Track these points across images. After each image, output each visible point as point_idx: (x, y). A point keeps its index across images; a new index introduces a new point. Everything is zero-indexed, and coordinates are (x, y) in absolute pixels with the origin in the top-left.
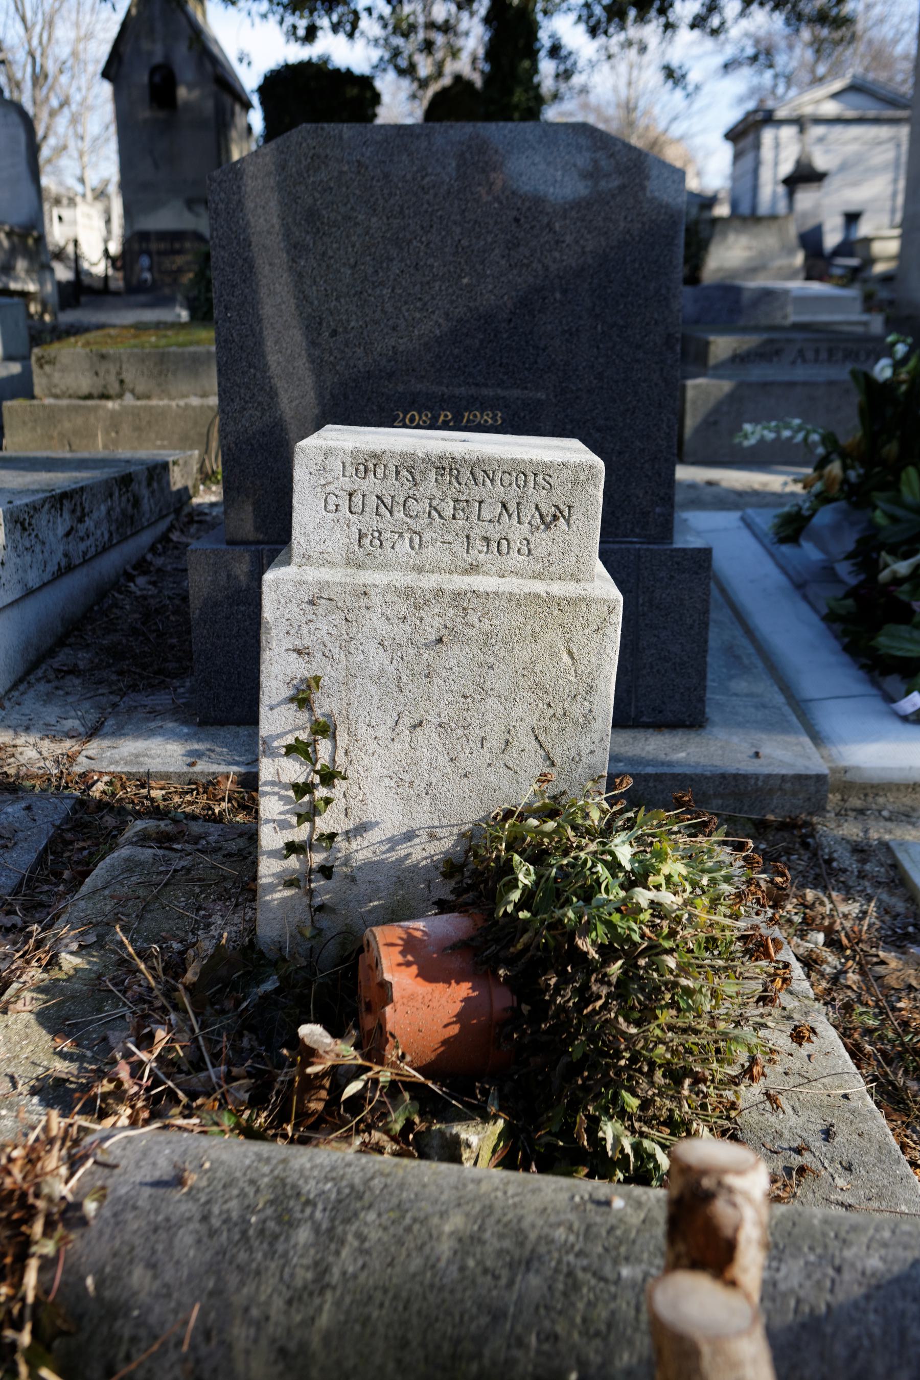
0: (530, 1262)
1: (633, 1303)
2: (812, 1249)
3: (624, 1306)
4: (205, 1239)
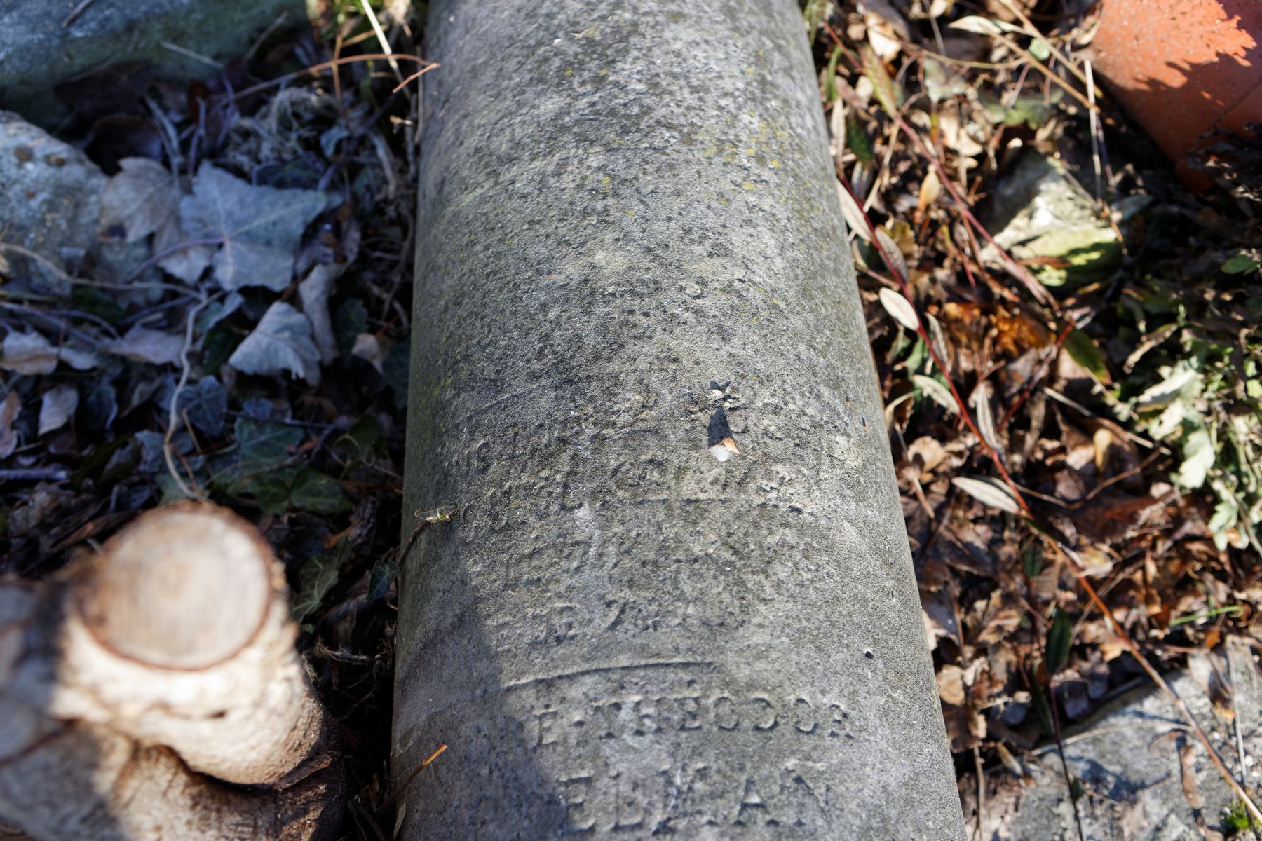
0: (569, 380)
1: (540, 544)
2: (702, 774)
3: (537, 533)
4: (523, 14)
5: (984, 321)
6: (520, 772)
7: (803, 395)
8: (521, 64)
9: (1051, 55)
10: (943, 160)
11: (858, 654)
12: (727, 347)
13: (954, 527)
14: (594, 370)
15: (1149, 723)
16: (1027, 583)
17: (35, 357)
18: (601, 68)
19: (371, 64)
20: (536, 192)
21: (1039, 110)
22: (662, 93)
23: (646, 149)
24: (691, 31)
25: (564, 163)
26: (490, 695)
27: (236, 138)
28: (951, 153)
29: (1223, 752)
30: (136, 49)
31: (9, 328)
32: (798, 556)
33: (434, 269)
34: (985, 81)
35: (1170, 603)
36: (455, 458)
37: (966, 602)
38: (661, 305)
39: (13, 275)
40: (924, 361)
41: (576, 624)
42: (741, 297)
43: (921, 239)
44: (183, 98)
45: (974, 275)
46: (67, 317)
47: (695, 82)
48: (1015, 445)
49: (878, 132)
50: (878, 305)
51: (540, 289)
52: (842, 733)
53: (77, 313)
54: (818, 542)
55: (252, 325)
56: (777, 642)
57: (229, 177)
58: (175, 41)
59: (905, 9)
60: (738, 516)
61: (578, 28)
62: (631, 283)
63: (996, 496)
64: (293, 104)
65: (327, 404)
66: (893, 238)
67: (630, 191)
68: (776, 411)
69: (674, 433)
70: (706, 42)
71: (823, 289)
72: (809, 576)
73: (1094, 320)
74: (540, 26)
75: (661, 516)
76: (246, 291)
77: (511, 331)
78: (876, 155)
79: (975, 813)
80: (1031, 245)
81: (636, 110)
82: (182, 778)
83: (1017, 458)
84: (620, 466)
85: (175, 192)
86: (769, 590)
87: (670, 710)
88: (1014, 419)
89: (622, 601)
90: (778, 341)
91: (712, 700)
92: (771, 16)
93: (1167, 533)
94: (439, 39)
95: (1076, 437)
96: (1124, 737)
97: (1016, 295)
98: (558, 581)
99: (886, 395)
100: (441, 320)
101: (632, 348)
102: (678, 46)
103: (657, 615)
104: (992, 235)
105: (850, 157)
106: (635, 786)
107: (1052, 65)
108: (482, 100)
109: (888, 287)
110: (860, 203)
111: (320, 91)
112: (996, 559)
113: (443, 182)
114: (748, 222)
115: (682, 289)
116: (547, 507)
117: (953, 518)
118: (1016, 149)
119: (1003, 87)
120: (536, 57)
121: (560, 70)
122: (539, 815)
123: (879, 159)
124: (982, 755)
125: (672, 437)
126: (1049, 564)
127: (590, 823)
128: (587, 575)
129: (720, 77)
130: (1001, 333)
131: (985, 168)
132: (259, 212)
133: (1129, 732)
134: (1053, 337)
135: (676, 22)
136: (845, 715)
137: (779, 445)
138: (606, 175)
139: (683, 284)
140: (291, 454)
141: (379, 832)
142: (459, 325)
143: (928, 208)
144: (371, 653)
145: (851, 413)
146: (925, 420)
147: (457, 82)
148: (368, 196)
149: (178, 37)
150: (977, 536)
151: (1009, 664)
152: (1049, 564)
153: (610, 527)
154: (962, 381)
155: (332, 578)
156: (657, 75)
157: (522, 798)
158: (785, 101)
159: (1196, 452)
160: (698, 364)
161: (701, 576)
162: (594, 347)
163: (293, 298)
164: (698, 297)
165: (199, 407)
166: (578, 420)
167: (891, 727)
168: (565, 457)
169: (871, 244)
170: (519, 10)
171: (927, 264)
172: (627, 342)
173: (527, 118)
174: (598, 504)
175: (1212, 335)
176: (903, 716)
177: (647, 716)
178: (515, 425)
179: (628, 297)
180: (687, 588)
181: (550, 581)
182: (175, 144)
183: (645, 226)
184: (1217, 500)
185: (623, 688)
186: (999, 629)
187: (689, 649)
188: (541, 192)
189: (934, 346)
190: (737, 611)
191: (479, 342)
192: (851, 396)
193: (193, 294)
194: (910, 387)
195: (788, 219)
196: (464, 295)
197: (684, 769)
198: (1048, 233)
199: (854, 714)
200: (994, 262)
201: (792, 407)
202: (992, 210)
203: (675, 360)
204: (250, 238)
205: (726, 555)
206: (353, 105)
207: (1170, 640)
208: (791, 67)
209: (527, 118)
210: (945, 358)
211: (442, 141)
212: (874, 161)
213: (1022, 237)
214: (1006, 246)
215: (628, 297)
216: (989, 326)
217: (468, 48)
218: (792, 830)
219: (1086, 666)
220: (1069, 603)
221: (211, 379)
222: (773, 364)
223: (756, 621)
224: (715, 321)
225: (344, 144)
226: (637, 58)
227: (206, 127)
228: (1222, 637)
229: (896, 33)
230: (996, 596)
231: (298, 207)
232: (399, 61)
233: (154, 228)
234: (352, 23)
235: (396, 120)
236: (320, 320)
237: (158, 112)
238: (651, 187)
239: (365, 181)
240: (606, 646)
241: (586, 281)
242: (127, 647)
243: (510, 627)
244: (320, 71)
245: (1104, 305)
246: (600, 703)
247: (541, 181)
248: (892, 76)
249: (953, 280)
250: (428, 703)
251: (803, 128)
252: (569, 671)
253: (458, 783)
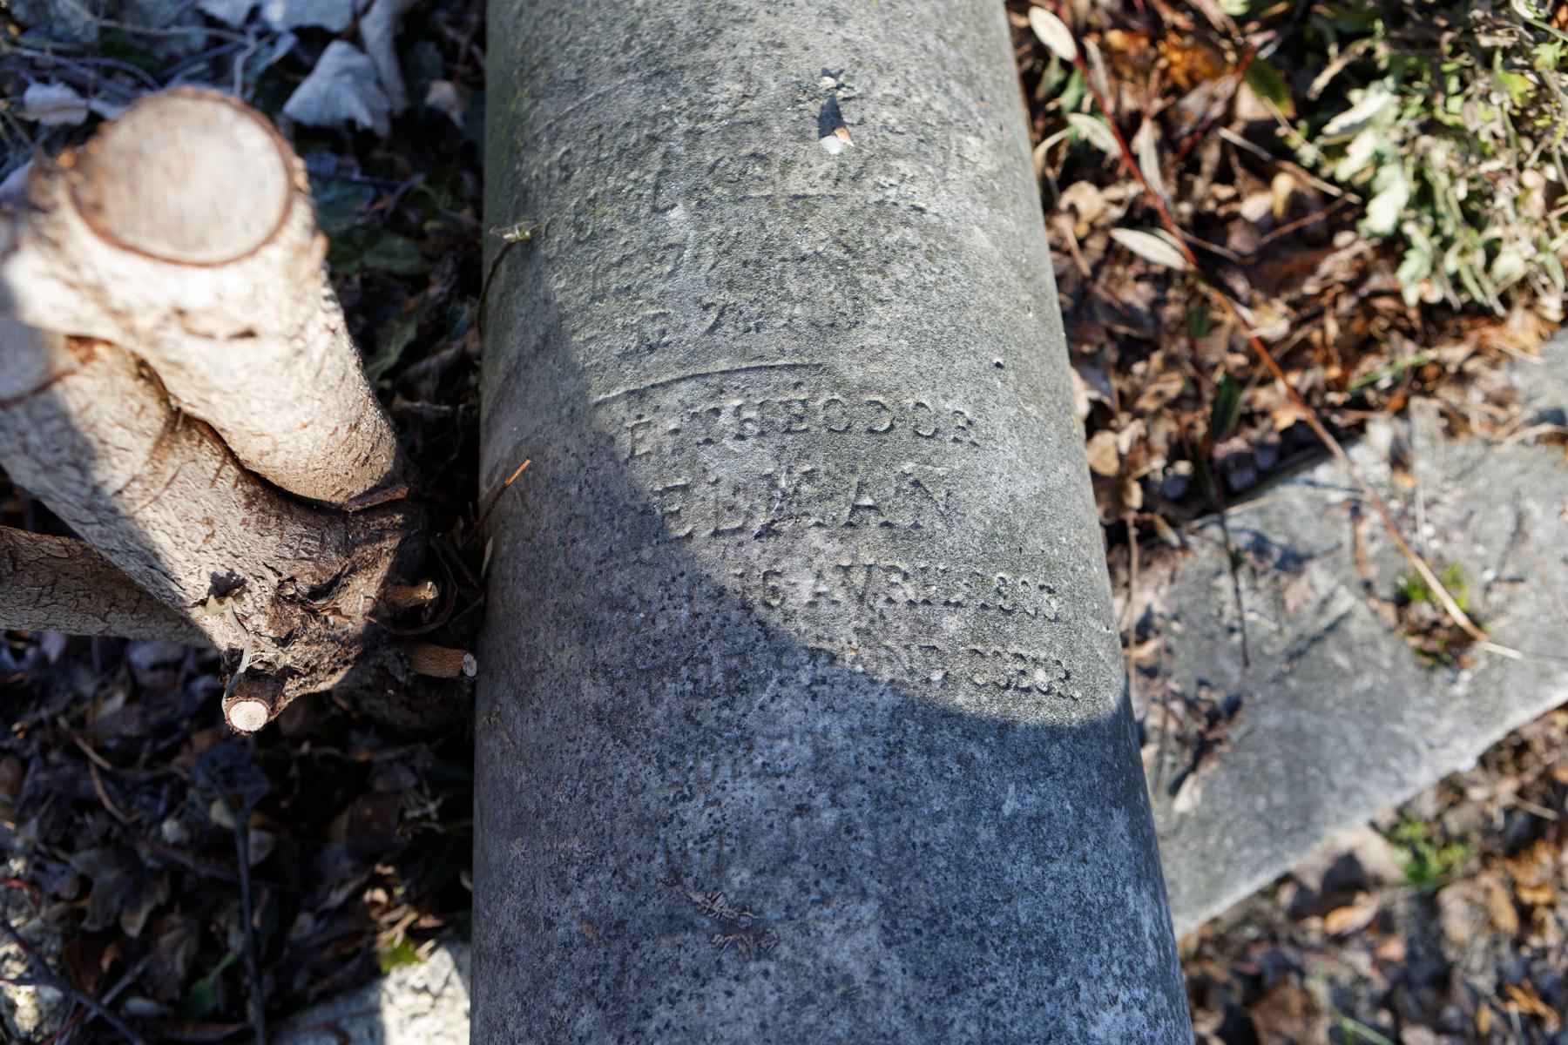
0: (660, 73)
1: (630, 251)
2: (809, 476)
3: (627, 238)
6: (611, 486)
7: (929, 89)
11: (987, 362)
12: (841, 32)
13: (1113, 286)
14: (688, 59)
15: (1320, 492)
16: (1193, 346)
17: (60, 108)
26: (577, 412)
29: (1400, 522)
31: (31, 80)
32: (919, 257)
35: (1349, 363)
36: (534, 173)
37: (1123, 368)
39: (32, 21)
40: (1081, 99)
41: (670, 330)
46: (97, 67)
48: (1184, 192)
50: (1029, 32)
52: (966, 439)
53: (109, 62)
54: (943, 243)
55: (307, 70)
56: (895, 344)
60: (852, 213)
63: (1161, 249)
65: (402, 162)
68: (897, 103)
69: (780, 124)
72: (933, 278)
73: (1280, 50)
75: (765, 213)
79: (1127, 585)
82: (231, 471)
83: (1186, 208)
84: (718, 162)
86: (886, 291)
87: (773, 413)
88: (1181, 156)
89: (721, 304)
91: (821, 402)
93: (1351, 287)
95: (1253, 182)
96: (1292, 507)
98: (650, 287)
101: (730, 33)
103: (760, 316)
106: (736, 491)
112: (1158, 320)
116: (636, 211)
117: (1112, 276)
122: (633, 526)
124: (1137, 525)
125: (777, 129)
126: (1217, 324)
127: (687, 530)
128: (682, 279)
130: (1171, 64)
133: (1298, 502)
134: (1230, 69)
136: (969, 422)
137: (900, 139)
140: (361, 214)
141: (465, 569)
142: (536, 27)
144: (455, 404)
145: (986, 114)
146: (1082, 164)
150: (1137, 295)
151: (1169, 435)
152: (1217, 324)
153: (707, 227)
155: (410, 333)
157: (614, 511)
159: (1385, 189)
161: (810, 275)
163: (354, 37)
166: (670, 115)
167: (1022, 439)
168: (656, 155)
174: (694, 204)
175: (1409, 44)
176: (1037, 430)
177: (749, 420)
178: (600, 126)
180: (793, 287)
181: (640, 288)
184: (1408, 244)
185: (722, 392)
186: (1160, 394)
187: (796, 351)
189: (1093, 78)
190: (849, 312)
192: (987, 97)
193: (239, 39)
197: (789, 472)
199: (980, 421)
201: (916, 100)
203: (781, 45)
205: (838, 253)
207: (1348, 405)
218: (907, 532)
219: (1254, 434)
220: (1240, 368)
222: (895, 52)
223: (872, 321)
228: (1406, 400)
230: (1157, 358)
236: (386, 63)
240: (703, 351)
242: (129, 238)
243: (597, 341)
245: (1290, 29)
246: (698, 410)
250: (512, 433)
252: (663, 379)
253: (546, 507)
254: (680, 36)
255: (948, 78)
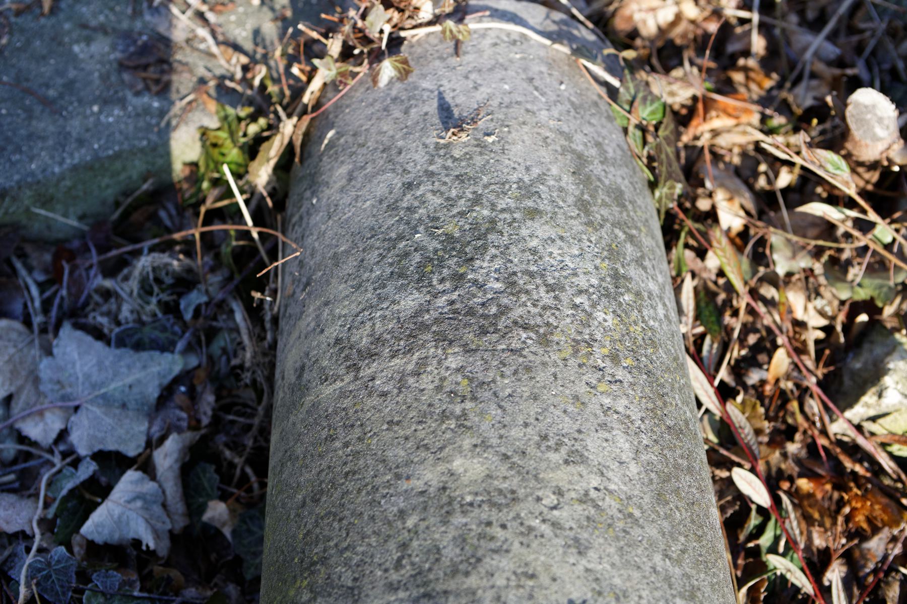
5: (836, 495)
8: (382, 257)
9: (894, 240)
10: (791, 334)
12: (584, 562)
18: (460, 266)
19: (233, 233)
20: (395, 391)
21: (885, 290)
22: (519, 292)
23: (503, 350)
24: (546, 227)
25: (423, 363)
27: (97, 298)
28: (800, 325)
30: (6, 213)
33: (293, 458)
34: (830, 256)
38: (518, 516)
42: (597, 507)
43: (772, 414)
44: (48, 257)
45: (824, 447)
47: (551, 281)
49: (728, 302)
50: (730, 481)
51: (398, 494)
55: (105, 492)
57: (89, 339)
58: (43, 205)
59: (751, 180)
61: (438, 224)
62: (489, 493)
64: (154, 269)
66: (743, 413)
67: (488, 394)
70: (561, 238)
71: (677, 491)
74: (401, 219)
76: (100, 457)
77: (369, 537)
78: (728, 337)
80: (881, 421)
81: (494, 310)
85: (36, 352)
90: (634, 553)
92: (624, 206)
94: (301, 218)
97: (867, 470)
99: (739, 573)
100: (298, 515)
101: (491, 562)
102: (534, 243)
104: (843, 411)
105: (700, 329)
107: (895, 249)
108: (343, 289)
109: (740, 465)
110: (711, 378)
111: (181, 256)
113: (303, 368)
114: (603, 426)
115: (539, 499)
118: (863, 323)
119: (849, 263)
120: (397, 251)
121: (420, 265)
123: (729, 330)
129: (575, 275)
131: (832, 340)
132: (116, 374)
135: (533, 219)
138: (464, 377)
139: (540, 493)
143: (777, 381)
147: (318, 267)
148: (224, 359)
149: (47, 202)
154: (815, 559)
156: (515, 273)
158: (638, 294)
160: (554, 580)
162: (452, 560)
163: (146, 466)
164: (554, 508)
165: (48, 577)
169: (721, 418)
170: (381, 202)
171: (778, 439)
172: (484, 556)
173: (387, 313)
179: (486, 507)
182: (37, 304)
183: (502, 432)
188: (400, 392)
191: (336, 545)
193: (48, 456)
194: (763, 567)
195: (642, 420)
196: (322, 492)
198: (896, 411)
200: (844, 435)
202: (841, 383)
203: (533, 576)
204: (106, 401)
206: (213, 270)
208: (642, 257)
209: (387, 313)
210: (798, 539)
211: (302, 324)
212: (723, 334)
213: (872, 413)
214: (856, 421)
215: (486, 507)
216: (841, 503)
217: (330, 233)
221: (62, 549)
222: (629, 578)
224: (572, 534)
225: (203, 308)
226: (494, 257)
227: (69, 288)
229: (742, 207)
231: (155, 370)
232: (260, 233)
233: (13, 389)
234: (216, 192)
235: (257, 295)
236: (172, 488)
237: (23, 272)
238: (508, 391)
239: (222, 344)
241: (444, 489)
244: (182, 237)
247: (400, 380)
248: (740, 249)
249: (803, 453)
251: (655, 319)
254: (446, 561)
255: (674, 596)
